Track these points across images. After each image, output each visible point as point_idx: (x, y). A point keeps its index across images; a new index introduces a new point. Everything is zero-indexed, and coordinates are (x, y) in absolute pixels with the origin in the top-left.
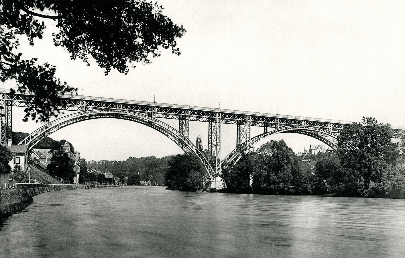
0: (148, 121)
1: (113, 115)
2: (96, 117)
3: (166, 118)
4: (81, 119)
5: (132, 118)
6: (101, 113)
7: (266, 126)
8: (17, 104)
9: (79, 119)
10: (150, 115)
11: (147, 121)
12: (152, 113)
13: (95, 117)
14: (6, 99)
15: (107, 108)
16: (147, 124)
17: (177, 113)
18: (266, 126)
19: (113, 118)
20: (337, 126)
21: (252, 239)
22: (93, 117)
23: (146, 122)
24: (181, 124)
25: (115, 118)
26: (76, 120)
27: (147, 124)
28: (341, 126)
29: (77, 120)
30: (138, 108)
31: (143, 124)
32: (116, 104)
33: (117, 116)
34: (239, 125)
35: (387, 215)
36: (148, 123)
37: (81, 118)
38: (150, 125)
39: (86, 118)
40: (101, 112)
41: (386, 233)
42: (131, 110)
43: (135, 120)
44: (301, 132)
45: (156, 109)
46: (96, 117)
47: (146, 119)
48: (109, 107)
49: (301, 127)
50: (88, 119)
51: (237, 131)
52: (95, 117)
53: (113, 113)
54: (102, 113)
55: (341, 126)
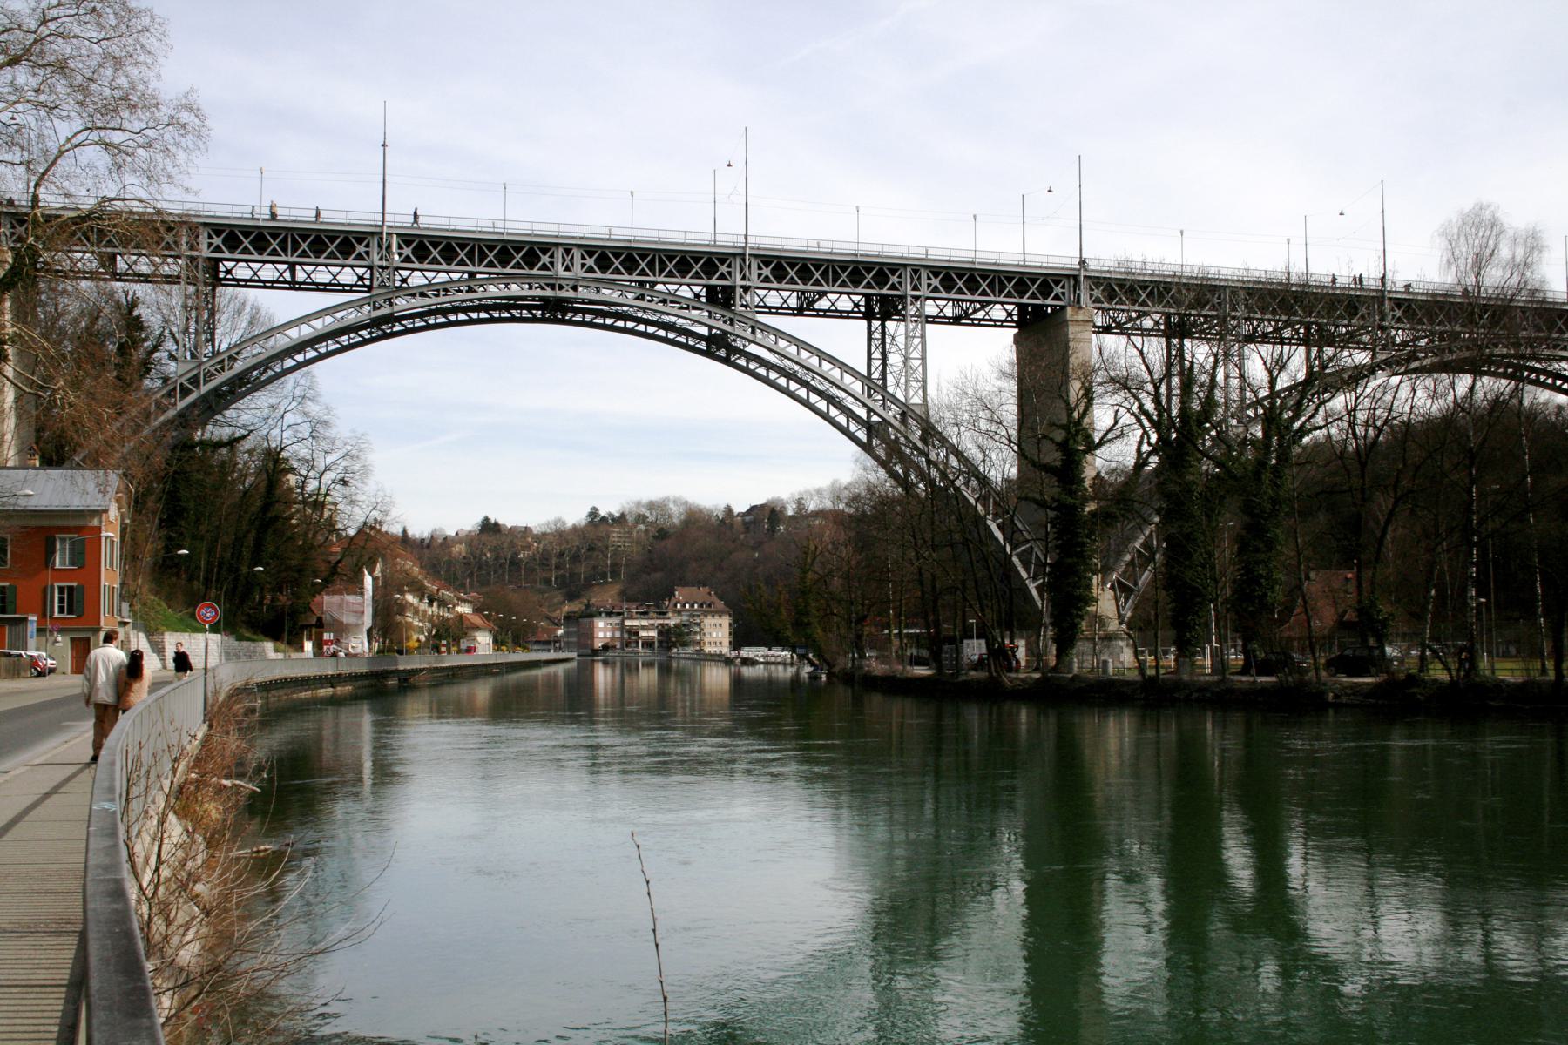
0: (711, 328)
1: (529, 308)
2: (443, 320)
3: (799, 311)
4: (370, 333)
5: (625, 321)
6: (471, 300)
7: (1176, 331)
8: (242, 272)
9: (363, 333)
10: (720, 298)
11: (704, 331)
12: (732, 289)
13: (441, 320)
14: (205, 252)
15: (508, 270)
16: (703, 346)
17: (539, 269)
18: (1176, 331)
19: (534, 320)
20: (960, 284)
21: (1249, 1016)
22: (432, 322)
23: (700, 337)
24: (879, 346)
25: (543, 320)
26: (346, 337)
27: (703, 346)
28: (984, 285)
29: (352, 335)
30: (483, 257)
31: (685, 347)
32: (546, 248)
33: (554, 311)
34: (876, 324)
35: (112, 779)
36: (709, 339)
37: (375, 323)
38: (722, 353)
39: (398, 328)
40: (530, 288)
41: (108, 899)
42: (626, 277)
43: (641, 328)
44: (1501, 370)
45: (578, 261)
46: (443, 320)
47: (701, 322)
48: (518, 266)
49: (542, 282)
50: (407, 331)
51: (869, 354)
52: (441, 320)
53: (533, 299)
54: (480, 299)
55: (984, 285)
